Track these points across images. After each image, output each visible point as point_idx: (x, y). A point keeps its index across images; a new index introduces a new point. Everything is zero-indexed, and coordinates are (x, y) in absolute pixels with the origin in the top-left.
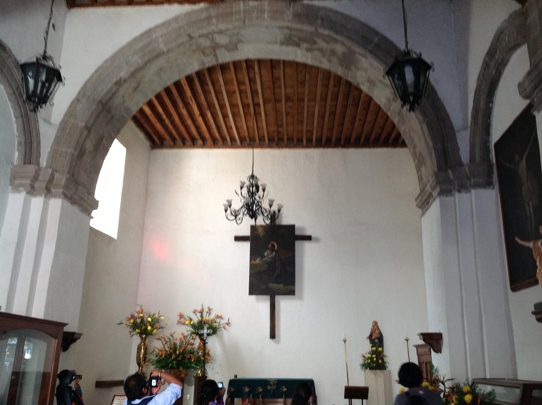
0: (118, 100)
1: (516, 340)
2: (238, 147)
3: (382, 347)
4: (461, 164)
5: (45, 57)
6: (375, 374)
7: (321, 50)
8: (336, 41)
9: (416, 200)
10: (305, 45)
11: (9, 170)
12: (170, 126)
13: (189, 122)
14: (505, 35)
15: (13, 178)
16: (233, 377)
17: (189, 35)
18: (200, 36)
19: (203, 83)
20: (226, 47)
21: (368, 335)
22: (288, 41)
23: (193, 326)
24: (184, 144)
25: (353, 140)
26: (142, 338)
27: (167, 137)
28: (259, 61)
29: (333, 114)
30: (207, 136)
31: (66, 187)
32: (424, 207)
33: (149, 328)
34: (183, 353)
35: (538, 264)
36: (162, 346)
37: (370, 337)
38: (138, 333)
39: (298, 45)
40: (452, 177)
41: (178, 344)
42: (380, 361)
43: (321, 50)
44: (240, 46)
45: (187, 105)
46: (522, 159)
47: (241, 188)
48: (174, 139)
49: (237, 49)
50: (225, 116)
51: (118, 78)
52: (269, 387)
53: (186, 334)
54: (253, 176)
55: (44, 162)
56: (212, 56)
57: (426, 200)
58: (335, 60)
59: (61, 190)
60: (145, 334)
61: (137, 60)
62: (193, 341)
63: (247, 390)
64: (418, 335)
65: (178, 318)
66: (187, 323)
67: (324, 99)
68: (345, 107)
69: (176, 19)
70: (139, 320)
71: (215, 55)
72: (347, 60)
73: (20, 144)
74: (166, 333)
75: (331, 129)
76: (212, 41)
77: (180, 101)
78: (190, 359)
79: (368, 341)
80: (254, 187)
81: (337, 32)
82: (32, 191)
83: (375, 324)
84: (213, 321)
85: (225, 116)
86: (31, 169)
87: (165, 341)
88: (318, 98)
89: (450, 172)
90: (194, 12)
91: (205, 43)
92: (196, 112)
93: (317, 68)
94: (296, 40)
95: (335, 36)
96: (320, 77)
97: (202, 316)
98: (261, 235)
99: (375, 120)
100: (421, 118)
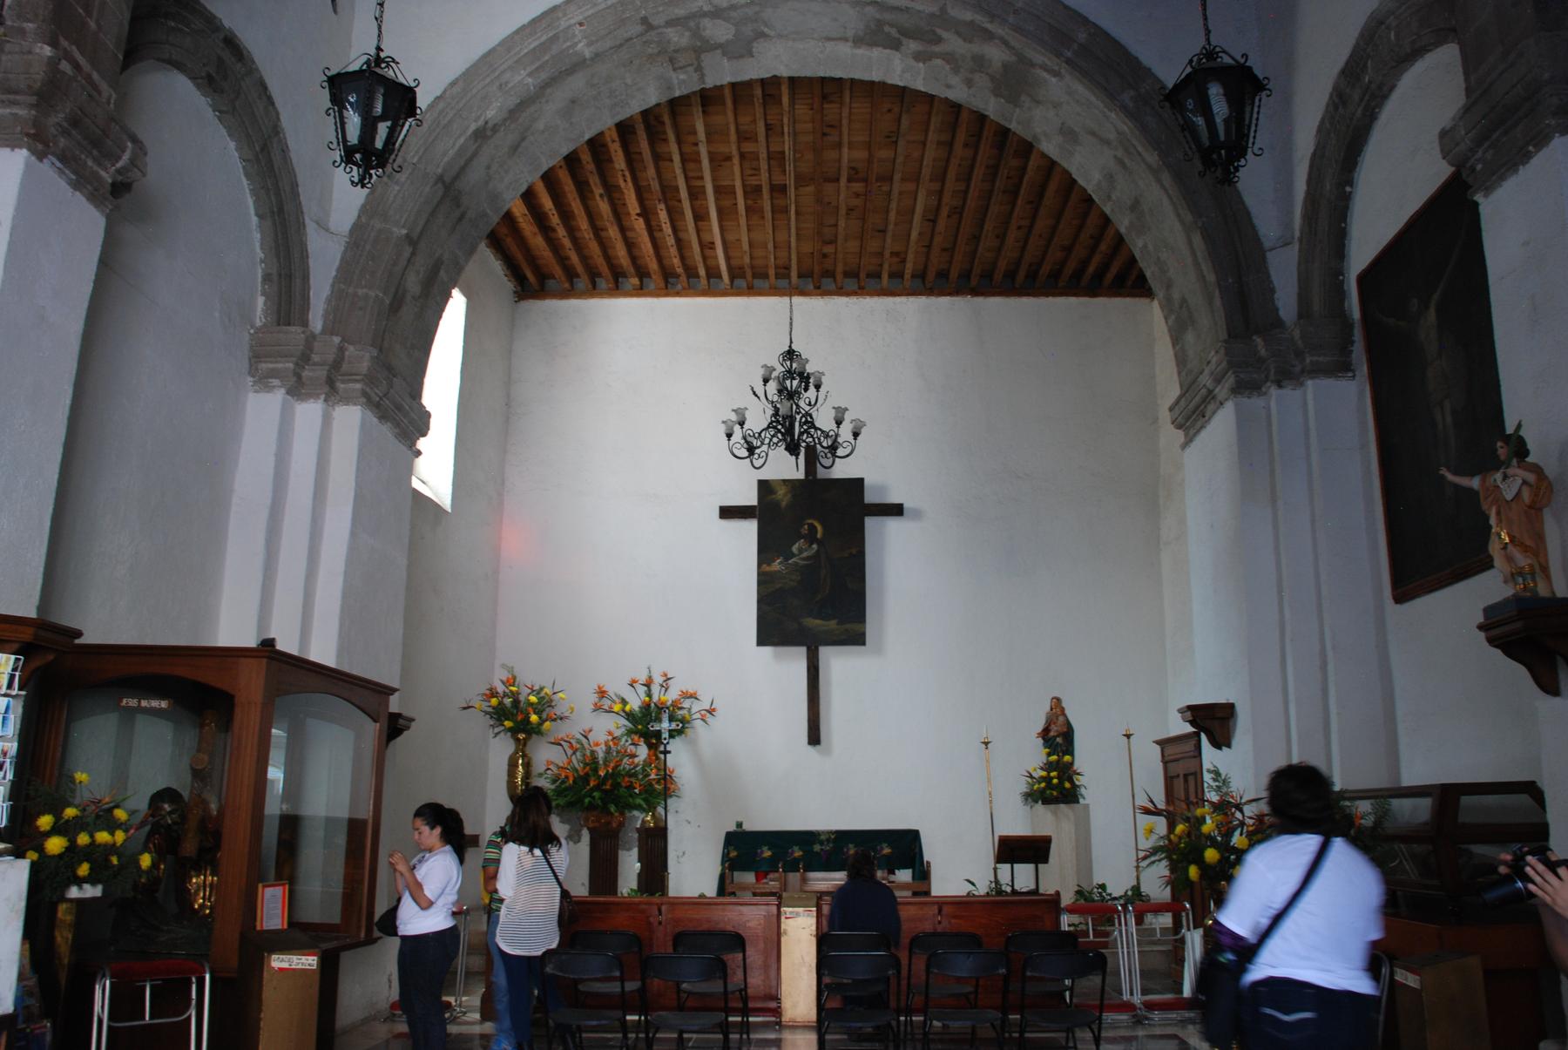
0: (475, 174)
1: (1401, 709)
3: (1072, 754)
4: (1279, 323)
5: (378, 60)
6: (1055, 813)
7: (949, 58)
8: (989, 36)
9: (1171, 409)
10: (913, 46)
11: (247, 337)
12: (567, 243)
13: (613, 232)
14: (1388, 28)
15: (257, 356)
16: (732, 828)
17: (644, 21)
19: (655, 137)
20: (725, 49)
21: (1040, 727)
23: (630, 716)
24: (594, 287)
25: (998, 276)
26: (518, 740)
27: (558, 271)
29: (958, 212)
30: (653, 266)
31: (370, 379)
33: (534, 718)
34: (615, 775)
35: (1493, 521)
36: (565, 759)
37: (1045, 733)
38: (510, 729)
39: (895, 45)
40: (1263, 352)
41: (601, 755)
42: (1067, 785)
43: (949, 58)
44: (758, 47)
45: (611, 191)
47: (766, 381)
48: (571, 274)
50: (700, 217)
51: (481, 122)
52: (817, 848)
53: (617, 733)
54: (790, 354)
55: (317, 322)
57: (1197, 407)
58: (981, 80)
61: (523, 79)
63: (767, 854)
64: (1181, 711)
65: (594, 698)
66: (617, 708)
67: (941, 177)
70: (508, 701)
71: (699, 69)
72: (1013, 82)
73: (267, 278)
74: (572, 730)
76: (696, 33)
77: (598, 180)
78: (630, 787)
79: (1040, 741)
80: (794, 378)
81: (993, 17)
82: (298, 390)
84: (676, 705)
86: (295, 333)
88: (926, 172)
89: (1259, 341)
91: (678, 38)
92: (633, 206)
93: (930, 99)
94: (894, 32)
97: (649, 695)
98: (784, 504)
99: (1054, 228)
100: (1189, 218)
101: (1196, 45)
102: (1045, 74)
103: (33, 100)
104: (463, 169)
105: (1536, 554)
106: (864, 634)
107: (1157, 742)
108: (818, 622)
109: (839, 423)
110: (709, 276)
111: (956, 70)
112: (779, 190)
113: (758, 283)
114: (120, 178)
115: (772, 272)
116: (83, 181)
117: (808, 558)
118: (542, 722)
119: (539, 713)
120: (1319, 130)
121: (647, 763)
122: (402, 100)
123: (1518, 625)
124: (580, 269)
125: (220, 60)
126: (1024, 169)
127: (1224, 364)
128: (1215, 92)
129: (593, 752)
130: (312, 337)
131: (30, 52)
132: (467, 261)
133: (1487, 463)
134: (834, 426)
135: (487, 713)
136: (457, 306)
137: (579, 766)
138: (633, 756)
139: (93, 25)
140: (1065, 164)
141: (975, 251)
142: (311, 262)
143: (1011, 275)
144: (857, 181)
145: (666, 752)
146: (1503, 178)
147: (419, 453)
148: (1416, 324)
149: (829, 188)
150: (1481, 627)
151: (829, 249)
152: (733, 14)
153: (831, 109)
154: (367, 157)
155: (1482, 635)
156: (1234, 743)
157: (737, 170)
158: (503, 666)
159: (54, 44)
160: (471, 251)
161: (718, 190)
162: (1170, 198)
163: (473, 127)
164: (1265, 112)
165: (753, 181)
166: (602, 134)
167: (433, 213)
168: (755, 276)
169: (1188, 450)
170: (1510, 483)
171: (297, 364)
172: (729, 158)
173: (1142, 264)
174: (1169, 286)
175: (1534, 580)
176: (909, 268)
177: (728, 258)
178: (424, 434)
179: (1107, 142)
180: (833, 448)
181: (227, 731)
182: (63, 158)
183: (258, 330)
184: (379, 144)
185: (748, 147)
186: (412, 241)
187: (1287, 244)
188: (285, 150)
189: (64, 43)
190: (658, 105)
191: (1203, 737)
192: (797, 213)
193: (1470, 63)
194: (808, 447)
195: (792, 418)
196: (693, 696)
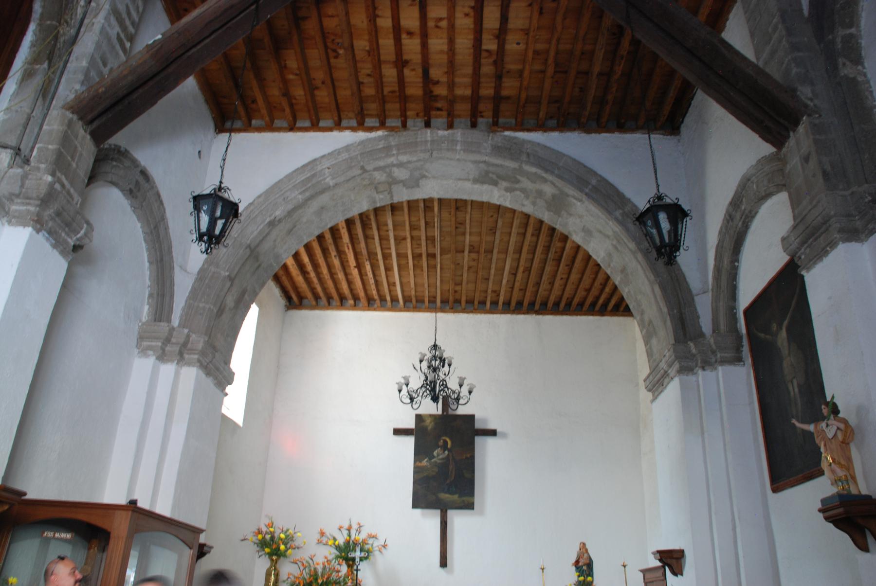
0: (267, 245)
2: (400, 310)
3: (592, 577)
4: (702, 335)
7: (523, 191)
8: (545, 180)
9: (645, 381)
10: (505, 184)
11: (137, 327)
12: (315, 280)
13: (341, 276)
14: (752, 182)
15: (141, 338)
17: (362, 168)
18: (376, 169)
19: (365, 226)
20: (404, 183)
22: (484, 178)
23: (338, 548)
24: (329, 303)
25: (550, 305)
26: (272, 560)
27: (309, 295)
28: (440, 200)
29: (528, 270)
30: (362, 294)
31: (203, 353)
32: (657, 390)
33: (282, 547)
35: (822, 450)
36: (299, 573)
37: (577, 563)
38: (268, 554)
39: (495, 184)
41: (320, 571)
43: (523, 191)
44: (422, 182)
45: (340, 253)
46: (781, 329)
47: (421, 361)
48: (317, 297)
49: (418, 186)
50: (388, 269)
51: (272, 218)
53: (330, 558)
54: (435, 347)
55: (176, 321)
56: (386, 193)
57: (659, 381)
58: (541, 203)
59: (196, 356)
60: (276, 554)
61: (297, 196)
62: (338, 567)
64: (653, 553)
65: (318, 536)
68: (544, 262)
69: (347, 148)
70: (268, 537)
71: (390, 193)
72: (557, 204)
73: (151, 295)
74: (303, 555)
75: (524, 290)
76: (390, 175)
79: (574, 568)
80: (437, 360)
81: (546, 171)
82: (162, 357)
83: (583, 545)
84: (364, 542)
85: (388, 269)
86: (163, 326)
87: (303, 565)
88: (511, 248)
89: (691, 345)
90: (369, 140)
91: (380, 177)
92: (352, 262)
93: (514, 211)
94: (494, 177)
95: (544, 175)
96: (516, 223)
98: (430, 428)
99: (581, 279)
100: (652, 277)
101: (652, 193)
102: (575, 201)
103: (38, 202)
104: (261, 241)
105: (848, 469)
106: (473, 504)
107: (642, 571)
108: (447, 495)
109: (461, 386)
110: (392, 300)
111: (527, 197)
112: (431, 256)
113: (419, 305)
114: (78, 243)
115: (426, 300)
116: (58, 244)
117: (442, 459)
118: (287, 550)
119: (286, 544)
120: (720, 232)
121: (347, 576)
122: (231, 210)
123: (841, 510)
124: (321, 294)
125: (137, 183)
126: (563, 249)
127: (673, 357)
128: (663, 217)
129: (315, 569)
130: (173, 329)
131: (41, 179)
132: (260, 290)
133: (817, 418)
134: (458, 387)
135: (255, 543)
136: (254, 311)
137: (307, 577)
138: (338, 571)
139: (74, 165)
140: (585, 247)
141: (537, 291)
142: (175, 288)
143: (557, 304)
144: (474, 252)
145: (357, 570)
146: (815, 263)
147: (226, 394)
148: (775, 336)
149: (459, 255)
150: (820, 511)
151: (458, 288)
152: (410, 166)
153: (460, 215)
154: (210, 239)
155: (821, 515)
156: (685, 573)
157: (409, 245)
158: (266, 516)
159: (53, 174)
160: (263, 285)
161: (399, 255)
162: (642, 267)
163: (268, 220)
164: (689, 231)
165: (417, 251)
166: (337, 224)
167: (243, 265)
168: (417, 301)
169: (654, 404)
170: (830, 429)
171: (163, 343)
172: (405, 239)
173: (628, 301)
174: (642, 313)
175: (848, 484)
176: (501, 299)
177: (403, 291)
178: (230, 383)
179: (608, 237)
180: (458, 399)
181: (104, 551)
182: (50, 233)
183: (143, 324)
184: (217, 232)
185: (415, 233)
186: (231, 279)
187: (704, 292)
188: (166, 228)
189: (58, 174)
190: (368, 211)
191: (667, 568)
192: (441, 269)
193: (795, 203)
194: (444, 397)
195: (435, 383)
196: (375, 537)
